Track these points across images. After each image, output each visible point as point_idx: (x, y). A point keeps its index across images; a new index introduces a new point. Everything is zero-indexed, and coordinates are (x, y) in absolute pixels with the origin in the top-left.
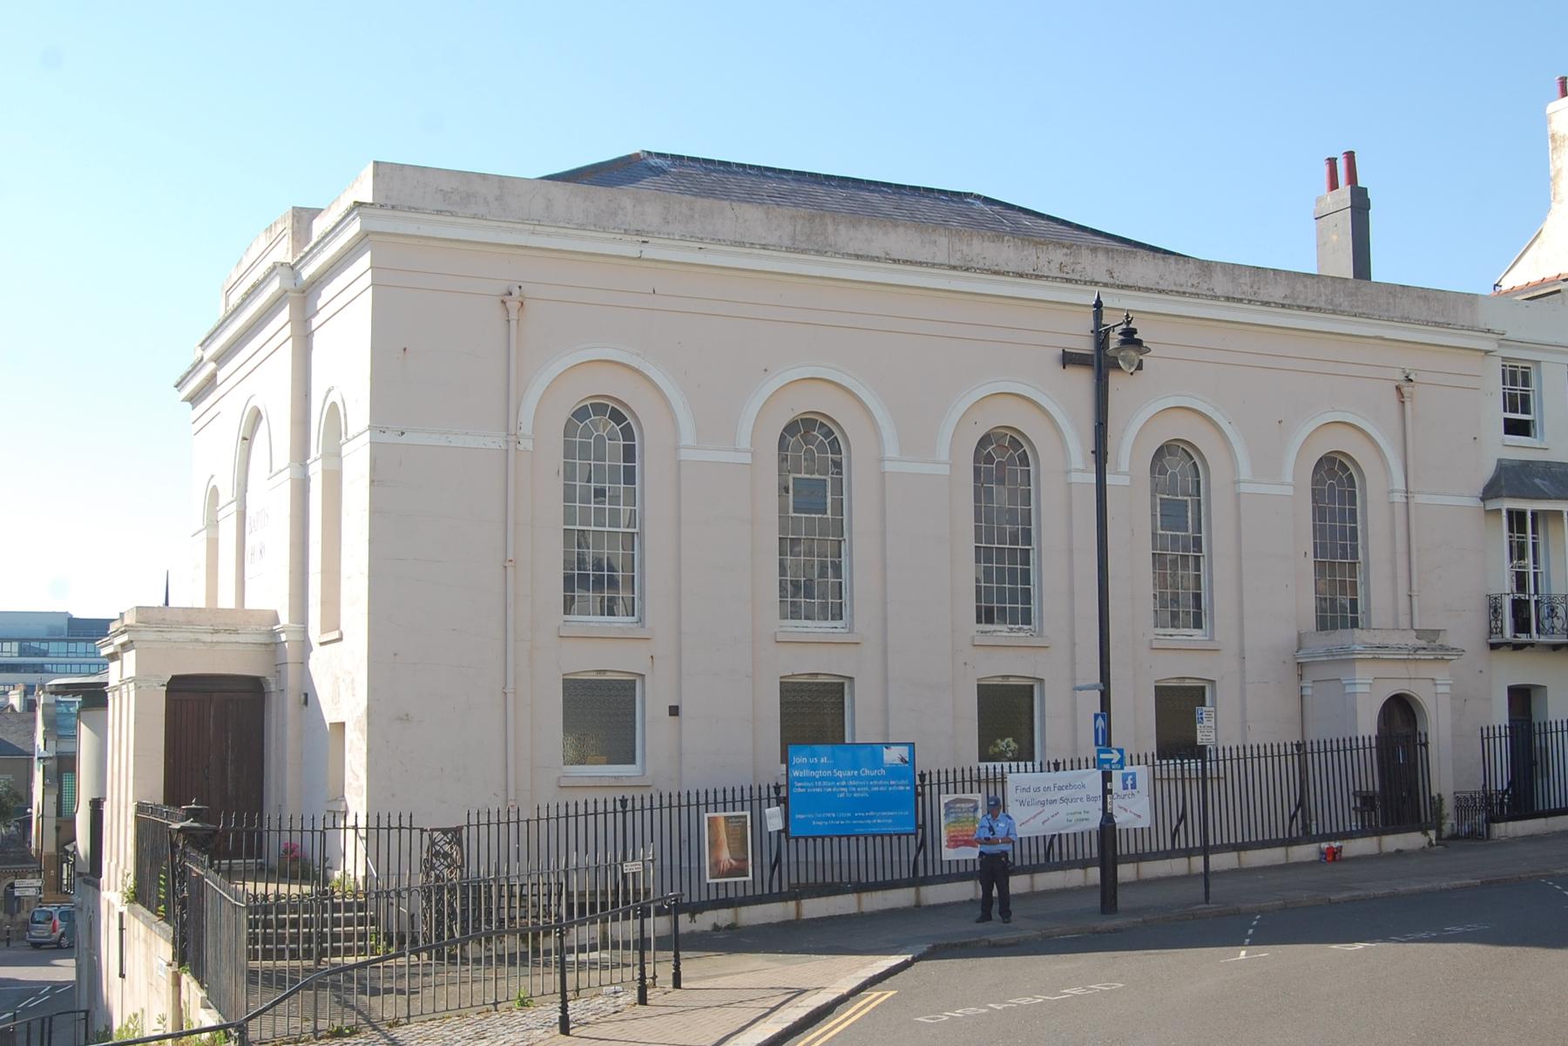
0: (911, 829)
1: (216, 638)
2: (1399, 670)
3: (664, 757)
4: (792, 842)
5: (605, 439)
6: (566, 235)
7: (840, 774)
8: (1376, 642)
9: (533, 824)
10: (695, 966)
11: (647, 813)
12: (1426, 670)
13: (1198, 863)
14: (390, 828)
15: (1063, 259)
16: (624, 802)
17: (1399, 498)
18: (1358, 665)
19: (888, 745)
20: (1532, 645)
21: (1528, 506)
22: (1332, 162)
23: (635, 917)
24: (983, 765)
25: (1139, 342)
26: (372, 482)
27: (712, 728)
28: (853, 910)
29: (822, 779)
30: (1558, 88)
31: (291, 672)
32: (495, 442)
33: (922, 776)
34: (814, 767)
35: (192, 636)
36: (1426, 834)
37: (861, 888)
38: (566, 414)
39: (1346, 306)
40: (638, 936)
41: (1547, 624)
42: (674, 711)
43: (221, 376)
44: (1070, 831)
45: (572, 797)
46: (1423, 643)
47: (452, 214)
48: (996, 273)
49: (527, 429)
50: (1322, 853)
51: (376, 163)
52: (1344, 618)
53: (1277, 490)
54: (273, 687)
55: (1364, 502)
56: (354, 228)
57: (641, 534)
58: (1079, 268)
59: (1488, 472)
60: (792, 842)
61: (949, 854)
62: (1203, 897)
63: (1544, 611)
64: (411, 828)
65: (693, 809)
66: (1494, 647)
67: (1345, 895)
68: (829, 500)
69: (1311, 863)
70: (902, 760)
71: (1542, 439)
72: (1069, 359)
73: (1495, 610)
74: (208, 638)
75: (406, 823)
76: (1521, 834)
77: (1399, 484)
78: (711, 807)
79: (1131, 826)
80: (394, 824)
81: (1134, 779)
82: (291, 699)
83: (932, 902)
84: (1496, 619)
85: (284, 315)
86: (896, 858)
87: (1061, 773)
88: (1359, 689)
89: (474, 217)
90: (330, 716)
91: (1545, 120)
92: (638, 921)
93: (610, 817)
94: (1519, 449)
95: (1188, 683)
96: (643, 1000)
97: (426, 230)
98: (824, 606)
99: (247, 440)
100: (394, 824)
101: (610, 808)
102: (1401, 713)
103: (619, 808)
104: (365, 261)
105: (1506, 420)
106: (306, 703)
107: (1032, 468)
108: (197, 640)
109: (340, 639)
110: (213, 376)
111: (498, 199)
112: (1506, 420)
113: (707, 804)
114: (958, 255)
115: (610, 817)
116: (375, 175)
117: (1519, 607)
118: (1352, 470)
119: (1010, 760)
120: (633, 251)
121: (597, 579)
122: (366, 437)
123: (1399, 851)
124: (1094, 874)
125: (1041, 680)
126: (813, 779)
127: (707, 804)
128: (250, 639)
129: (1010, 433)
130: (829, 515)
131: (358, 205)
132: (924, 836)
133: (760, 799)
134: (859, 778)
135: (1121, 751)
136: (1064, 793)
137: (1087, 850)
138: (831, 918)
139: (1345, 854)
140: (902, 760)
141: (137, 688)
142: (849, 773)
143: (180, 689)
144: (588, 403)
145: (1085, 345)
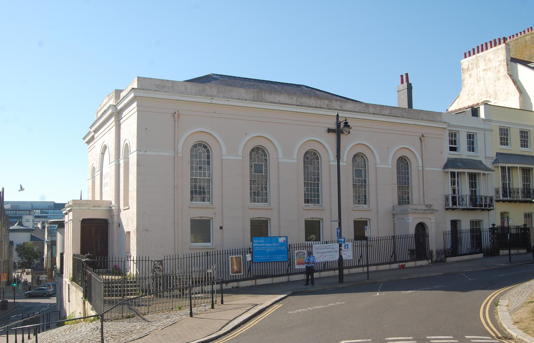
0: (287, 260)
1: (95, 208)
3: (219, 240)
5: (202, 153)
7: (267, 245)
8: (414, 208)
10: (227, 298)
15: (327, 103)
16: (207, 253)
17: (420, 168)
19: (280, 237)
20: (457, 209)
22: (402, 76)
24: (306, 242)
25: (349, 126)
27: (232, 231)
31: (115, 218)
32: (171, 154)
33: (290, 245)
37: (273, 276)
38: (191, 146)
41: (461, 203)
42: (221, 228)
45: (193, 252)
46: (427, 208)
51: (138, 77)
52: (405, 202)
56: (132, 95)
57: (212, 179)
59: (445, 161)
61: (297, 267)
63: (461, 199)
65: (226, 255)
67: (406, 278)
72: (330, 131)
73: (447, 199)
74: (92, 208)
75: (147, 259)
77: (421, 165)
82: (115, 225)
83: (292, 280)
85: (113, 119)
87: (328, 244)
88: (410, 221)
89: (165, 92)
90: (126, 230)
93: (204, 257)
94: (454, 155)
95: (363, 220)
97: (152, 96)
98: (262, 199)
99: (103, 154)
100: (144, 259)
101: (204, 255)
102: (421, 227)
104: (135, 104)
110: (93, 136)
115: (204, 257)
116: (138, 80)
117: (454, 198)
118: (408, 161)
120: (209, 101)
121: (200, 192)
122: (136, 153)
123: (421, 266)
124: (337, 272)
126: (259, 246)
134: (272, 246)
135: (344, 238)
139: (406, 266)
141: (73, 222)
145: (334, 127)
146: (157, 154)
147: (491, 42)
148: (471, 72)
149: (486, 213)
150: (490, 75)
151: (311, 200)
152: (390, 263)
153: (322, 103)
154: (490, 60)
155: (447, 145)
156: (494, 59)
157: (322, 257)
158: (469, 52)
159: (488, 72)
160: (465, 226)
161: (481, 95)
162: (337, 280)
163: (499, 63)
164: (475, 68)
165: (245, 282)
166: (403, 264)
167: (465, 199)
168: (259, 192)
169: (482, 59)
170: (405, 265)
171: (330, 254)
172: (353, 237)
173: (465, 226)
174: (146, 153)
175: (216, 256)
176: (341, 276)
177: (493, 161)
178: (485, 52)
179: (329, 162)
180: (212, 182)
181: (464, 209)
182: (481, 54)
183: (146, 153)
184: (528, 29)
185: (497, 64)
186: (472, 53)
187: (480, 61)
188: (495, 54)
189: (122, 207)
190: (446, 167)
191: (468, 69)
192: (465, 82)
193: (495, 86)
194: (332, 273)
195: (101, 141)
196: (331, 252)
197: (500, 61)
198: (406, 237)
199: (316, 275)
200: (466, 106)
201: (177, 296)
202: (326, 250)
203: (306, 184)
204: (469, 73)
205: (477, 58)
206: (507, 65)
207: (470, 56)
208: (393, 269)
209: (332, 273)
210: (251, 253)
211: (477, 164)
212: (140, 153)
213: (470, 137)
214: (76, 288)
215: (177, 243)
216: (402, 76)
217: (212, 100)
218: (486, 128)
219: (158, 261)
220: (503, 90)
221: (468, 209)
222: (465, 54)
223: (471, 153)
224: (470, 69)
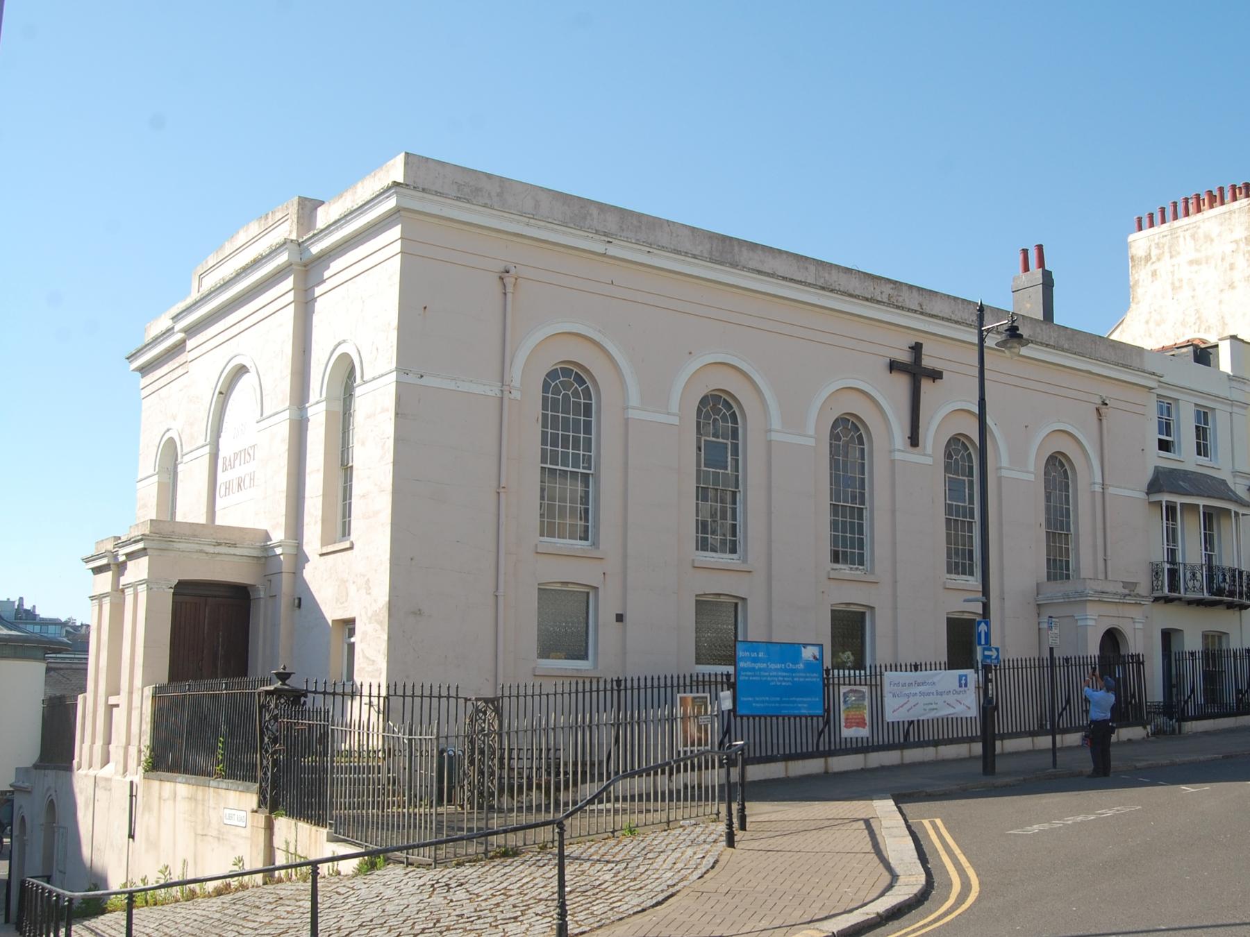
0: (820, 712)
2: (1111, 610)
3: (608, 655)
4: (738, 719)
5: (569, 402)
7: (773, 666)
8: (1099, 589)
9: (552, 698)
10: (759, 811)
11: (636, 692)
13: (1045, 742)
14: (440, 697)
15: (891, 292)
17: (1098, 489)
18: (1088, 605)
19: (805, 645)
20: (1180, 599)
21: (1179, 500)
22: (1025, 252)
25: (1020, 336)
26: (397, 414)
27: (649, 631)
28: (1030, 747)
29: (760, 670)
31: (286, 579)
32: (493, 391)
34: (755, 660)
35: (197, 547)
37: (787, 758)
39: (1066, 346)
40: (724, 781)
41: (1190, 584)
42: (620, 618)
43: (190, 344)
44: (924, 718)
46: (1127, 591)
47: (468, 202)
48: (851, 295)
51: (407, 154)
53: (1024, 476)
54: (262, 594)
55: (1076, 490)
56: (391, 203)
59: (1149, 475)
60: (738, 719)
61: (847, 733)
63: (1189, 576)
64: (457, 698)
65: (669, 690)
66: (1156, 599)
69: (1078, 747)
70: (814, 657)
72: (894, 366)
74: (211, 549)
75: (453, 693)
76: (1200, 730)
77: (1098, 479)
78: (682, 689)
79: (964, 716)
80: (444, 693)
82: (284, 602)
83: (836, 770)
85: (289, 283)
87: (918, 673)
88: (1090, 623)
89: (485, 206)
90: (332, 613)
91: (1126, 246)
92: (724, 771)
94: (1166, 461)
95: (966, 616)
96: (731, 842)
98: (723, 542)
99: (224, 394)
100: (444, 693)
102: (1112, 638)
104: (396, 232)
106: (299, 606)
107: (866, 447)
108: (201, 551)
109: (351, 548)
110: (183, 342)
113: (678, 686)
116: (406, 164)
117: (1173, 573)
118: (1067, 467)
119: (849, 669)
120: (599, 247)
122: (393, 376)
123: (1129, 740)
124: (978, 748)
125: (872, 608)
126: (753, 669)
127: (678, 686)
130: (729, 471)
131: (396, 184)
132: (828, 718)
133: (672, 687)
135: (997, 650)
136: (922, 689)
138: (774, 780)
140: (814, 657)
141: (149, 589)
142: (779, 666)
143: (185, 591)
145: (905, 357)
146: (452, 385)
147: (1234, 187)
148: (1154, 267)
149: (1233, 615)
151: (845, 553)
152: (1032, 734)
153: (878, 291)
154: (1209, 239)
155: (1154, 436)
156: (1220, 235)
157: (907, 707)
158: (1151, 216)
160: (1192, 642)
161: (1184, 324)
162: (979, 766)
163: (1234, 246)
164: (1167, 255)
165: (1018, 740)
168: (718, 525)
169: (1188, 234)
172: (944, 658)
173: (1192, 642)
174: (423, 382)
175: (649, 691)
176: (989, 757)
178: (1194, 218)
179: (892, 451)
180: (597, 483)
181: (1190, 602)
182: (1183, 221)
183: (423, 382)
186: (1157, 217)
187: (1181, 240)
188: (1221, 224)
191: (1148, 258)
193: (1220, 302)
194: (960, 750)
196: (928, 694)
197: (1236, 242)
199: (714, 777)
200: (1181, 340)
201: (625, 799)
203: (835, 509)
204: (1150, 267)
205: (1173, 231)
207: (1152, 225)
209: (960, 750)
210: (732, 686)
211: (1218, 488)
212: (413, 379)
213: (1203, 416)
214: (187, 783)
215: (499, 652)
216: (1025, 252)
221: (1200, 603)
222: (1140, 220)
223: (1202, 460)
224: (1154, 258)
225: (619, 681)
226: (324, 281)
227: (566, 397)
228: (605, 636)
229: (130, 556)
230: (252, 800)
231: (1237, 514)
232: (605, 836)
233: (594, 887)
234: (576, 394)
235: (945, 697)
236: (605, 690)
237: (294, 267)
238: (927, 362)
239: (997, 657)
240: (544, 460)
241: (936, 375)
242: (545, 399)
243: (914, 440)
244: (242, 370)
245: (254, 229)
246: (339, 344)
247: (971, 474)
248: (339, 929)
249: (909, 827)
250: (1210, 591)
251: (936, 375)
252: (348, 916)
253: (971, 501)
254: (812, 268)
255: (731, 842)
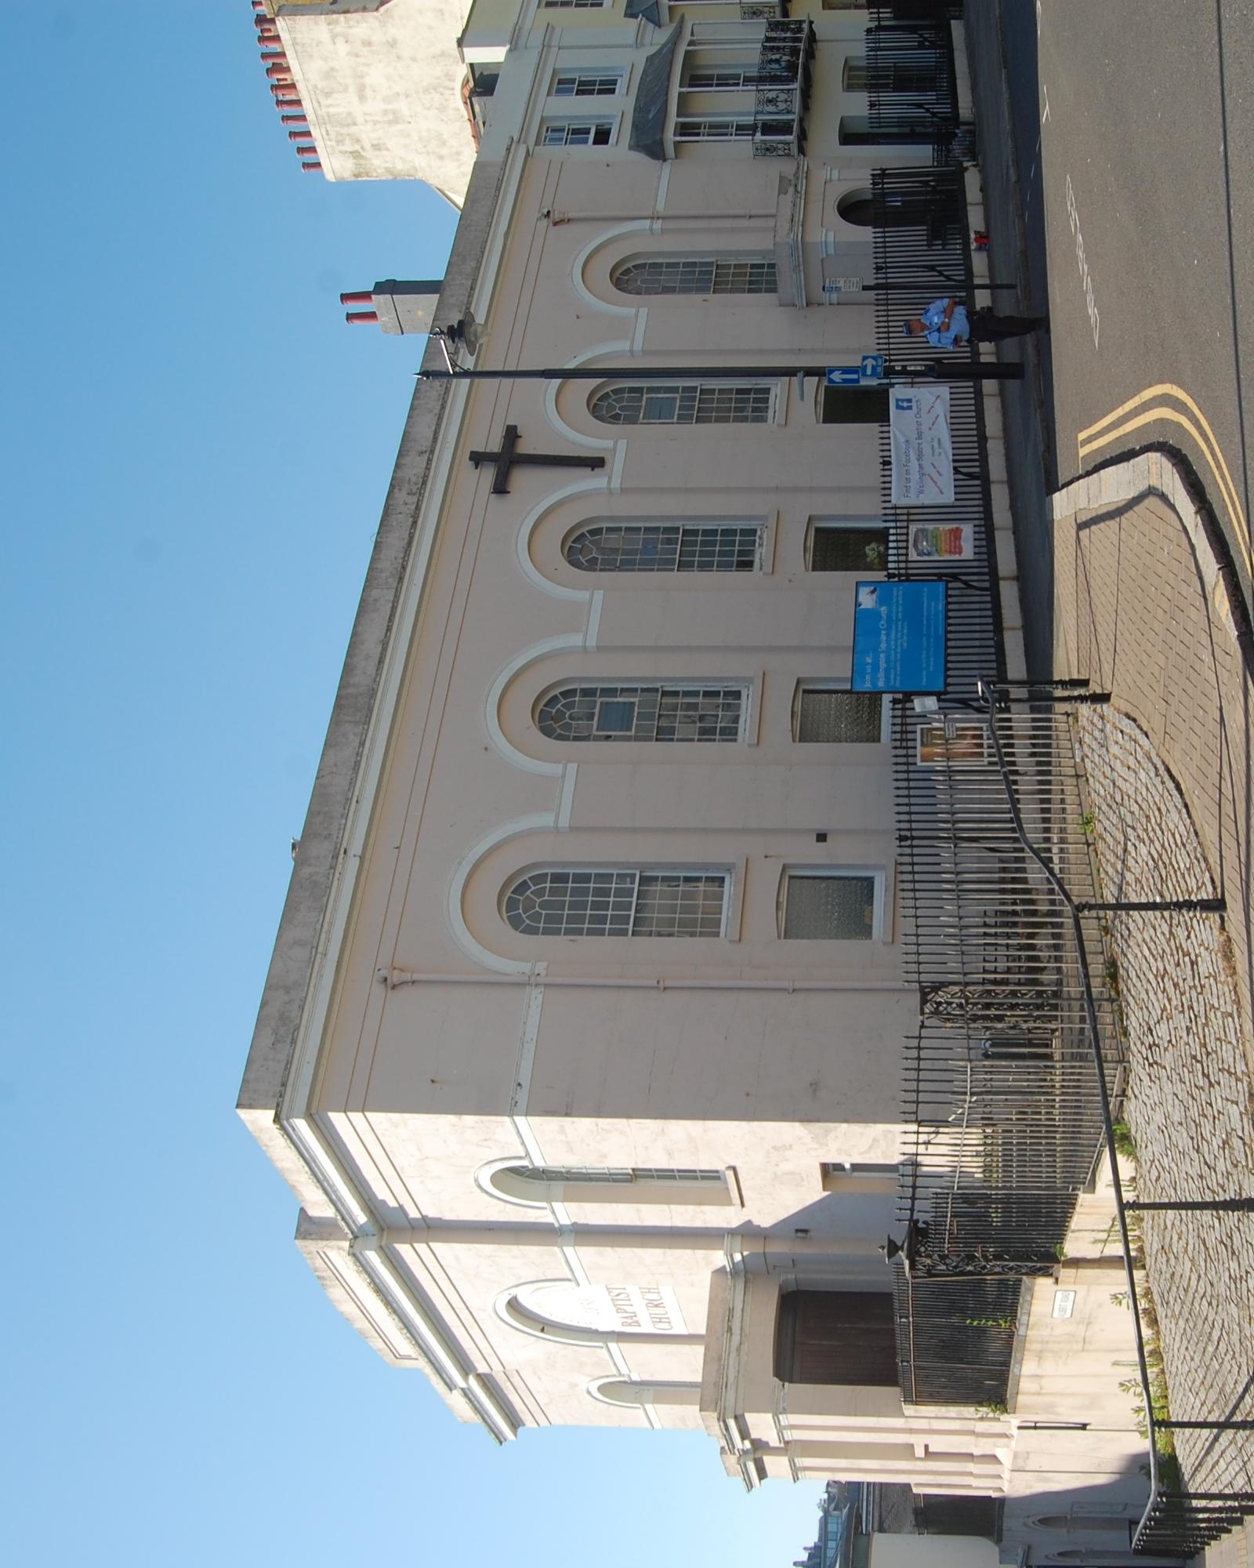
0: (941, 586)
1: (736, 1330)
3: (868, 852)
4: (949, 689)
6: (331, 924)
7: (883, 646)
8: (787, 225)
9: (920, 921)
12: (816, 187)
14: (919, 1059)
15: (404, 493)
17: (658, 225)
18: (809, 239)
19: (857, 604)
20: (801, 121)
22: (350, 317)
23: (1007, 710)
25: (461, 323)
26: (567, 1115)
27: (839, 802)
29: (887, 662)
30: (313, 171)
31: (776, 1248)
32: (536, 996)
35: (733, 1356)
36: (966, 169)
37: (998, 627)
38: (518, 934)
39: (473, 264)
41: (782, 106)
42: (822, 837)
43: (482, 1368)
44: (950, 452)
46: (791, 190)
49: (526, 967)
50: (979, 249)
51: (238, 1106)
52: (768, 274)
56: (301, 1125)
57: (643, 866)
58: (413, 479)
59: (640, 157)
60: (949, 689)
61: (968, 552)
62: (1012, 291)
64: (920, 1037)
65: (912, 776)
67: (1012, 171)
68: (621, 700)
69: (989, 257)
70: (873, 592)
71: (614, 117)
73: (768, 150)
74: (736, 1339)
79: (948, 402)
81: (903, 401)
82: (802, 1249)
83: (1015, 567)
84: (775, 149)
85: (404, 1250)
86: (977, 643)
88: (831, 238)
90: (814, 1191)
91: (341, 183)
92: (1014, 706)
93: (916, 851)
96: (1105, 698)
97: (311, 1055)
102: (851, 210)
103: (908, 843)
104: (337, 1119)
105: (595, 143)
106: (805, 1231)
107: (605, 525)
108: (738, 1350)
109: (734, 1169)
110: (480, 1377)
111: (287, 990)
112: (595, 143)
114: (391, 580)
115: (916, 851)
116: (251, 1107)
117: (768, 129)
119: (887, 548)
120: (353, 864)
122: (520, 1120)
124: (989, 385)
126: (887, 670)
127: (907, 764)
128: (739, 1297)
129: (569, 544)
130: (636, 700)
132: (948, 576)
135: (865, 358)
137: (976, 516)
138: (1025, 645)
139: (982, 229)
140: (873, 592)
141: (784, 1411)
143: (785, 1370)
144: (505, 915)
148: (367, 146)
149: (823, 51)
150: (376, 76)
151: (741, 553)
154: (330, 74)
155: (589, 150)
156: (325, 59)
157: (935, 476)
158: (301, 150)
159: (368, 81)
160: (858, 105)
161: (442, 109)
162: (1013, 385)
163: (340, 40)
164: (353, 130)
166: (973, 236)
167: (771, 95)
168: (701, 713)
169: (324, 102)
170: (976, 232)
171: (927, 451)
172: (875, 427)
173: (858, 105)
174: (526, 1084)
175: (914, 809)
177: (651, 26)
178: (303, 92)
182: (308, 108)
183: (526, 1084)
184: (280, 103)
185: (342, 48)
186: (303, 142)
187: (332, 110)
188: (311, 56)
189: (726, 1217)
190: (655, 150)
192: (399, 166)
193: (414, 59)
195: (490, 1325)
197: (334, 37)
198: (881, 248)
200: (464, 113)
202: (914, 464)
204: (369, 153)
206: (346, 12)
207: (312, 150)
208: (1006, 429)
210: (908, 697)
213: (563, 85)
215: (863, 985)
216: (350, 317)
217: (351, 853)
218: (540, 41)
219: (924, 1002)
220: (430, 28)
222: (306, 165)
224: (357, 147)
225: (901, 838)
226: (401, 1206)
227: (543, 905)
228: (845, 856)
229: (744, 1434)
230: (1043, 1284)
231: (691, 43)
232: (1092, 854)
233: (1156, 867)
234: (539, 893)
235: (924, 428)
236: (914, 882)
237: (383, 1243)
238: (495, 446)
239: (874, 358)
240: (624, 933)
241: (512, 434)
242: (546, 932)
243: (596, 463)
244: (514, 1305)
245: (336, 1293)
246: (480, 1187)
247: (640, 390)
248: (1201, 1177)
249: (1088, 474)
250: (792, 80)
251: (512, 434)
252: (1186, 1166)
253: (675, 390)
254: (375, 593)
255: (1105, 698)
